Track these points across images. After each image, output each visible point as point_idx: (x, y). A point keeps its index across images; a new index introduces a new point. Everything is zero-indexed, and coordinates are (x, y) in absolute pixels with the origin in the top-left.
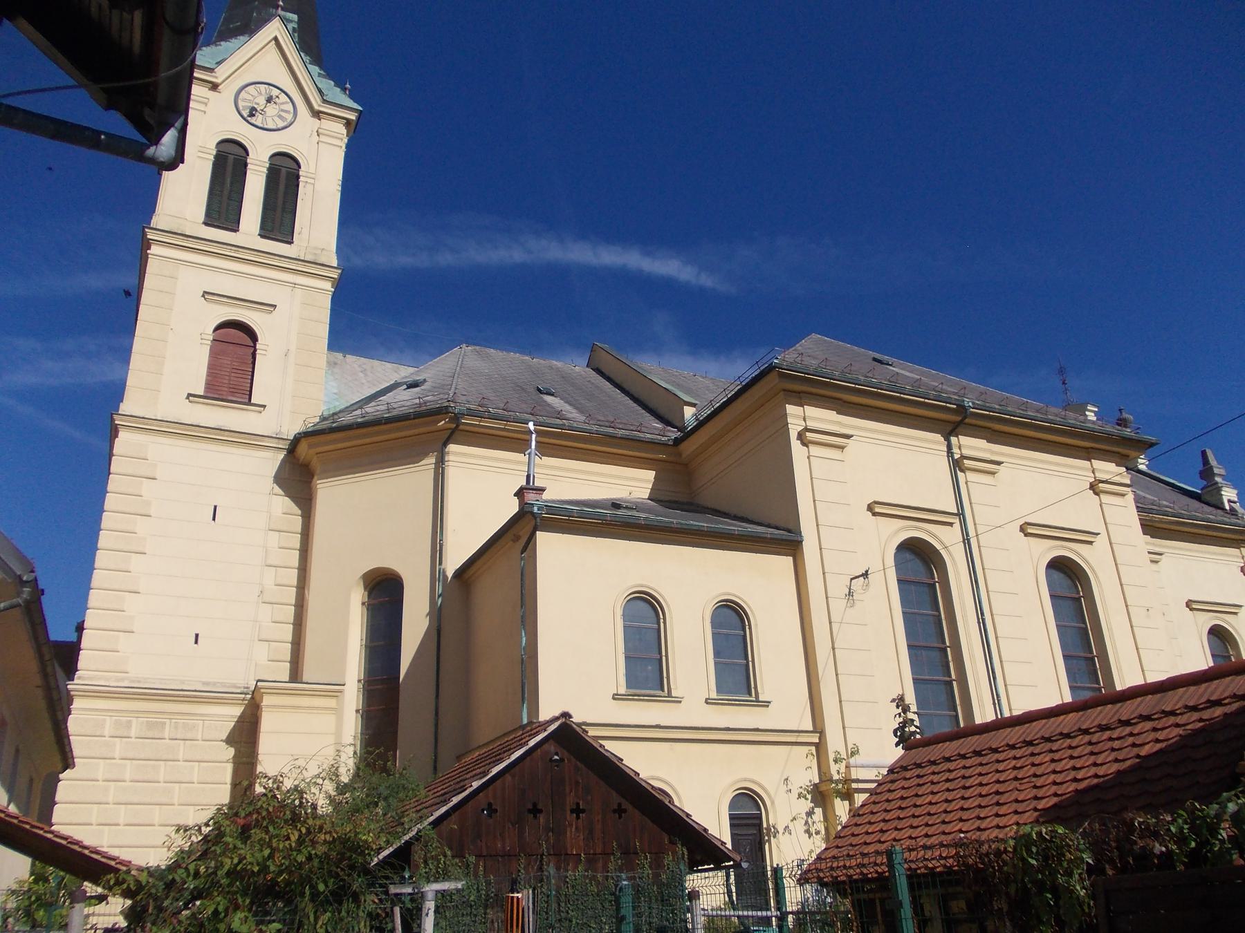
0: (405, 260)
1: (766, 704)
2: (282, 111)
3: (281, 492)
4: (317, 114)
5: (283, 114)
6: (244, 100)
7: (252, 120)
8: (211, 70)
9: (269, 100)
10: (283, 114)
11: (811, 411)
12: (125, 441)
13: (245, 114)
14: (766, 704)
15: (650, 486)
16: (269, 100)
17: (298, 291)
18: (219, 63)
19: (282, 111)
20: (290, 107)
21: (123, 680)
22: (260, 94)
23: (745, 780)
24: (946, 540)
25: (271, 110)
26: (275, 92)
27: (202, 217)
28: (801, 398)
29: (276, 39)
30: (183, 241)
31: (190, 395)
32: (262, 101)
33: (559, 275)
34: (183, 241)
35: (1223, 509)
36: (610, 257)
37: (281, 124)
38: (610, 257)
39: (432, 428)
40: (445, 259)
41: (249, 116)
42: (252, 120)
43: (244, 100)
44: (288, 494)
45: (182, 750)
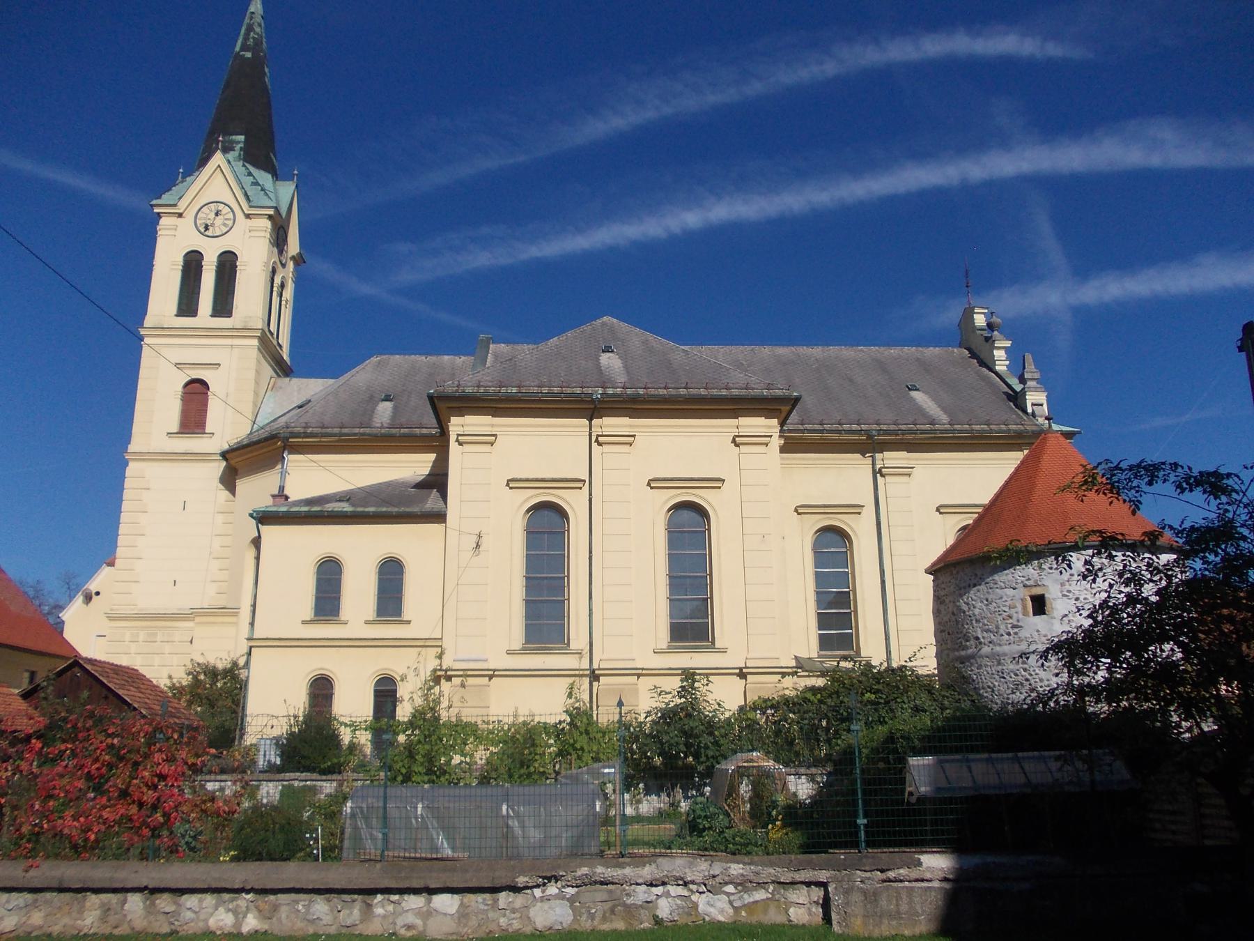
0: (713, 98)
1: (409, 622)
2: (226, 219)
3: (223, 488)
4: (248, 216)
5: (226, 222)
6: (201, 219)
7: (207, 233)
8: (175, 205)
9: (217, 214)
10: (226, 222)
11: (469, 419)
12: (133, 469)
13: (203, 230)
14: (409, 622)
15: (431, 465)
16: (217, 214)
17: (236, 351)
18: (180, 198)
19: (226, 219)
20: (231, 216)
21: (133, 610)
22: (211, 211)
23: (386, 669)
24: (573, 502)
25: (219, 221)
26: (221, 206)
27: (174, 310)
28: (461, 412)
29: (219, 166)
30: (162, 330)
31: (169, 433)
32: (212, 215)
33: (883, 77)
34: (162, 330)
35: (1025, 411)
36: (934, 46)
37: (225, 230)
38: (934, 46)
39: (275, 447)
40: (755, 88)
41: (205, 231)
42: (207, 233)
43: (201, 219)
44: (228, 490)
45: (167, 648)
